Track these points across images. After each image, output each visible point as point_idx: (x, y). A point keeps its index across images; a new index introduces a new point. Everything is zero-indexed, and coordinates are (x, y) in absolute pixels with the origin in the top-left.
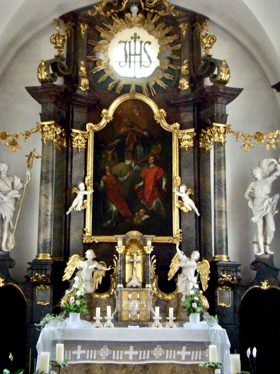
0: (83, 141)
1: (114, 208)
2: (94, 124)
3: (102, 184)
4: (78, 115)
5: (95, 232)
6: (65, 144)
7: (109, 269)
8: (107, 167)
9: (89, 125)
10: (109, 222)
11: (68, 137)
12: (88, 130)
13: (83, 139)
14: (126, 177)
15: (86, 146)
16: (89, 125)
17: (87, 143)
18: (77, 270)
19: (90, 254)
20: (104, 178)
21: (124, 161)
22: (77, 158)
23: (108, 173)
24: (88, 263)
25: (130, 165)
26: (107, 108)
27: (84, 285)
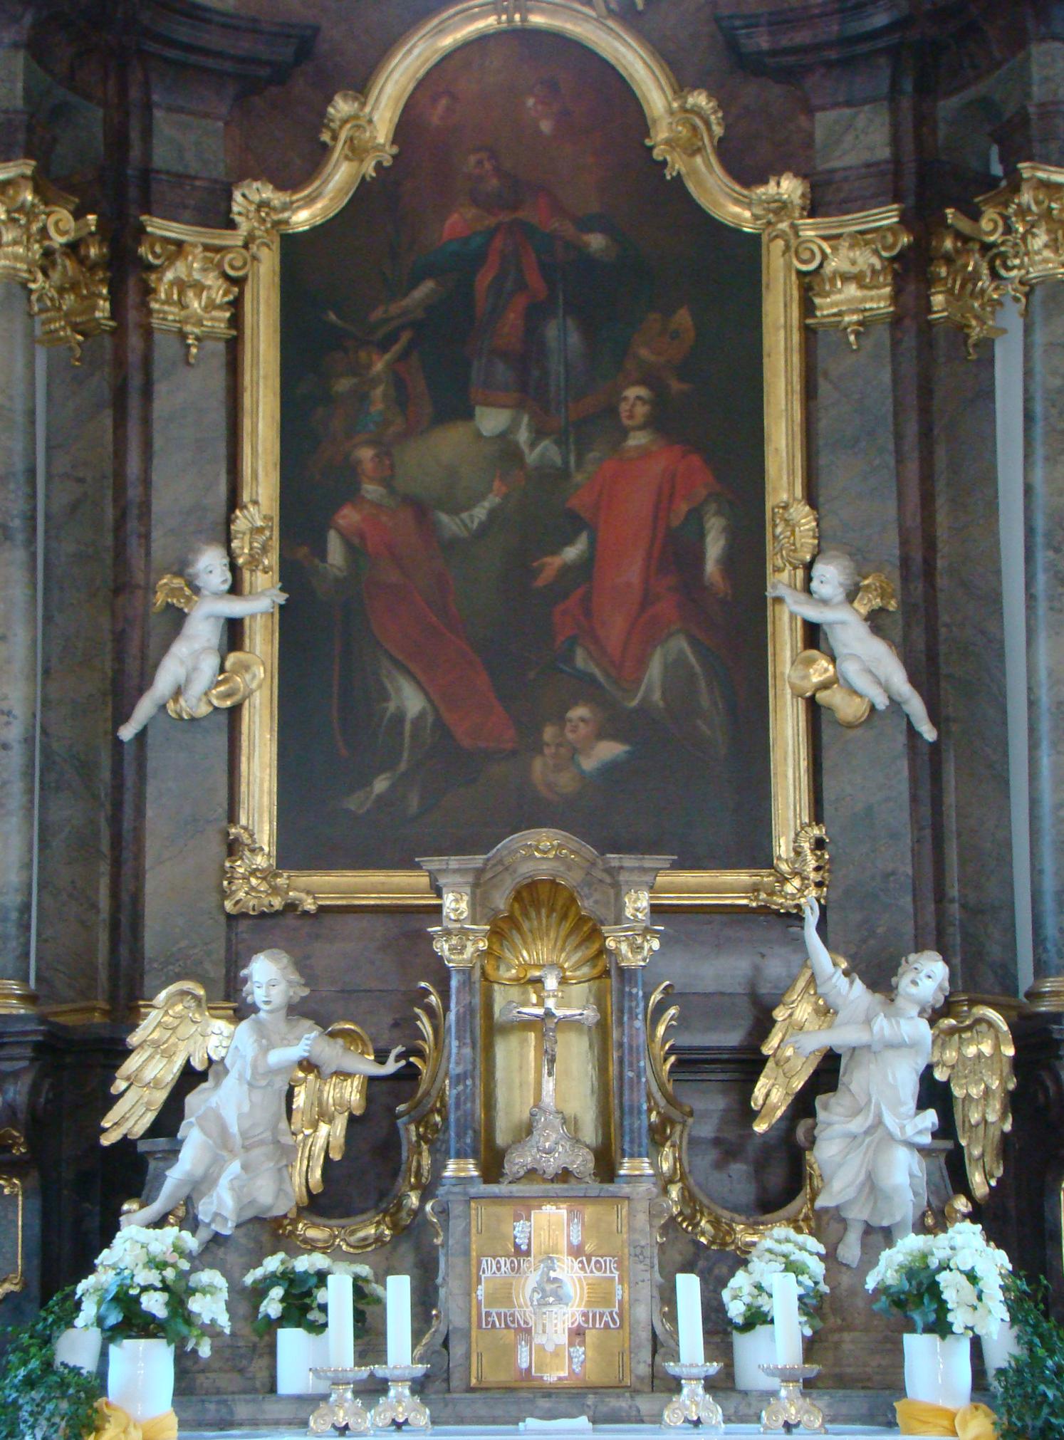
0: (218, 291)
1: (410, 700)
2: (280, 187)
3: (336, 553)
4: (182, 136)
5: (298, 848)
6: (103, 308)
7: (391, 1067)
8: (366, 454)
9: (250, 196)
10: (381, 785)
11: (125, 267)
12: (244, 226)
13: (214, 286)
14: (480, 513)
15: (236, 321)
16: (250, 196)
17: (236, 305)
18: (190, 1078)
19: (267, 976)
20: (349, 516)
21: (468, 415)
22: (182, 396)
23: (371, 490)
24: (261, 1031)
25: (504, 437)
26: (361, 87)
27: (235, 1167)
